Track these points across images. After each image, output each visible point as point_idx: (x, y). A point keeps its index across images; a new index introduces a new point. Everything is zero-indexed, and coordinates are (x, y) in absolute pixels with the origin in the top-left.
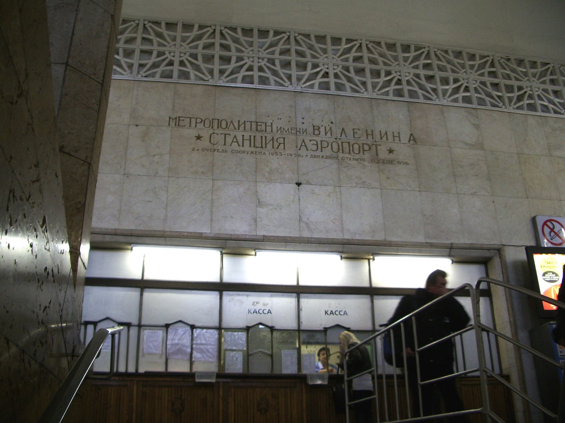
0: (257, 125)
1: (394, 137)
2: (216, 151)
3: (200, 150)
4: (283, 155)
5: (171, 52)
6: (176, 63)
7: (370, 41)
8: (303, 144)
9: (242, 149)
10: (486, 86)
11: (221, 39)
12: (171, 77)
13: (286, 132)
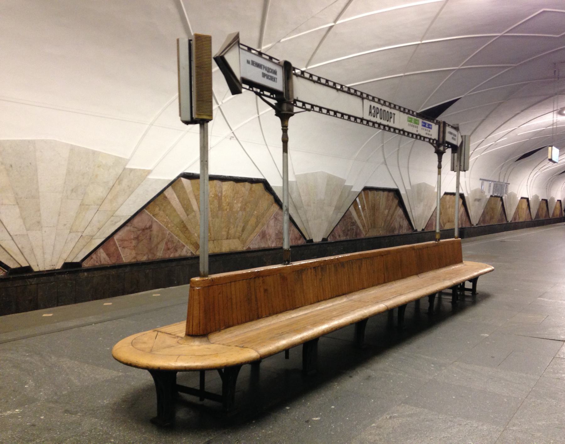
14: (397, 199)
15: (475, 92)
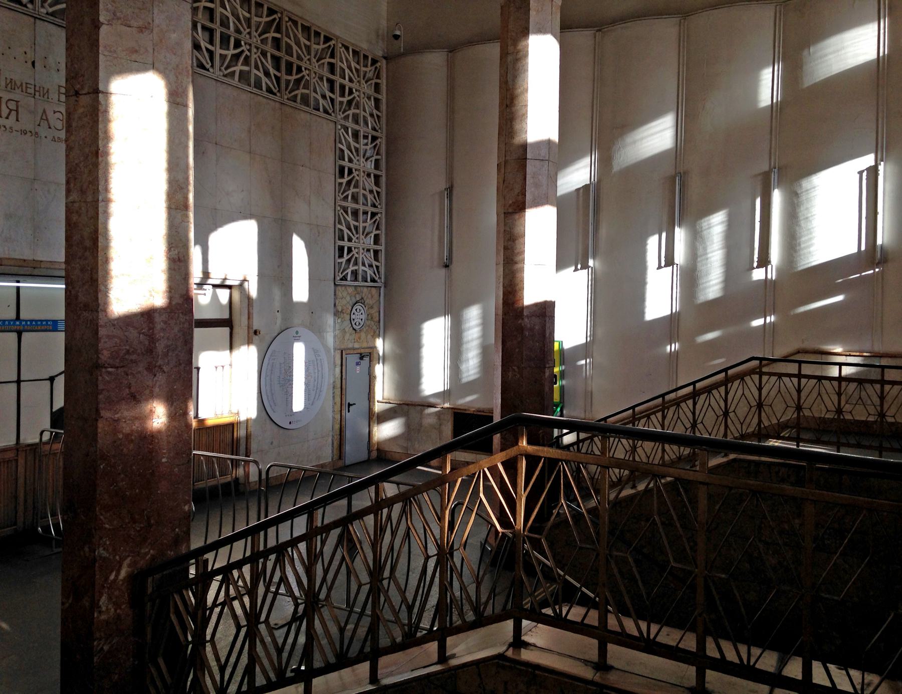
6: (350, 244)
10: (346, 212)
13: (18, 88)
15: (530, 480)
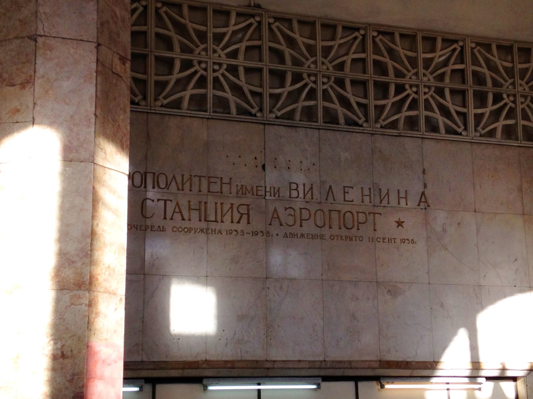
0: (209, 183)
1: (399, 198)
2: (149, 230)
3: (224, 233)
4: (245, 234)
5: (417, 88)
7: (274, 18)
8: (177, 210)
9: (186, 224)
11: (156, 26)
12: (179, 108)
14: (146, 202)
15: (225, 80)
